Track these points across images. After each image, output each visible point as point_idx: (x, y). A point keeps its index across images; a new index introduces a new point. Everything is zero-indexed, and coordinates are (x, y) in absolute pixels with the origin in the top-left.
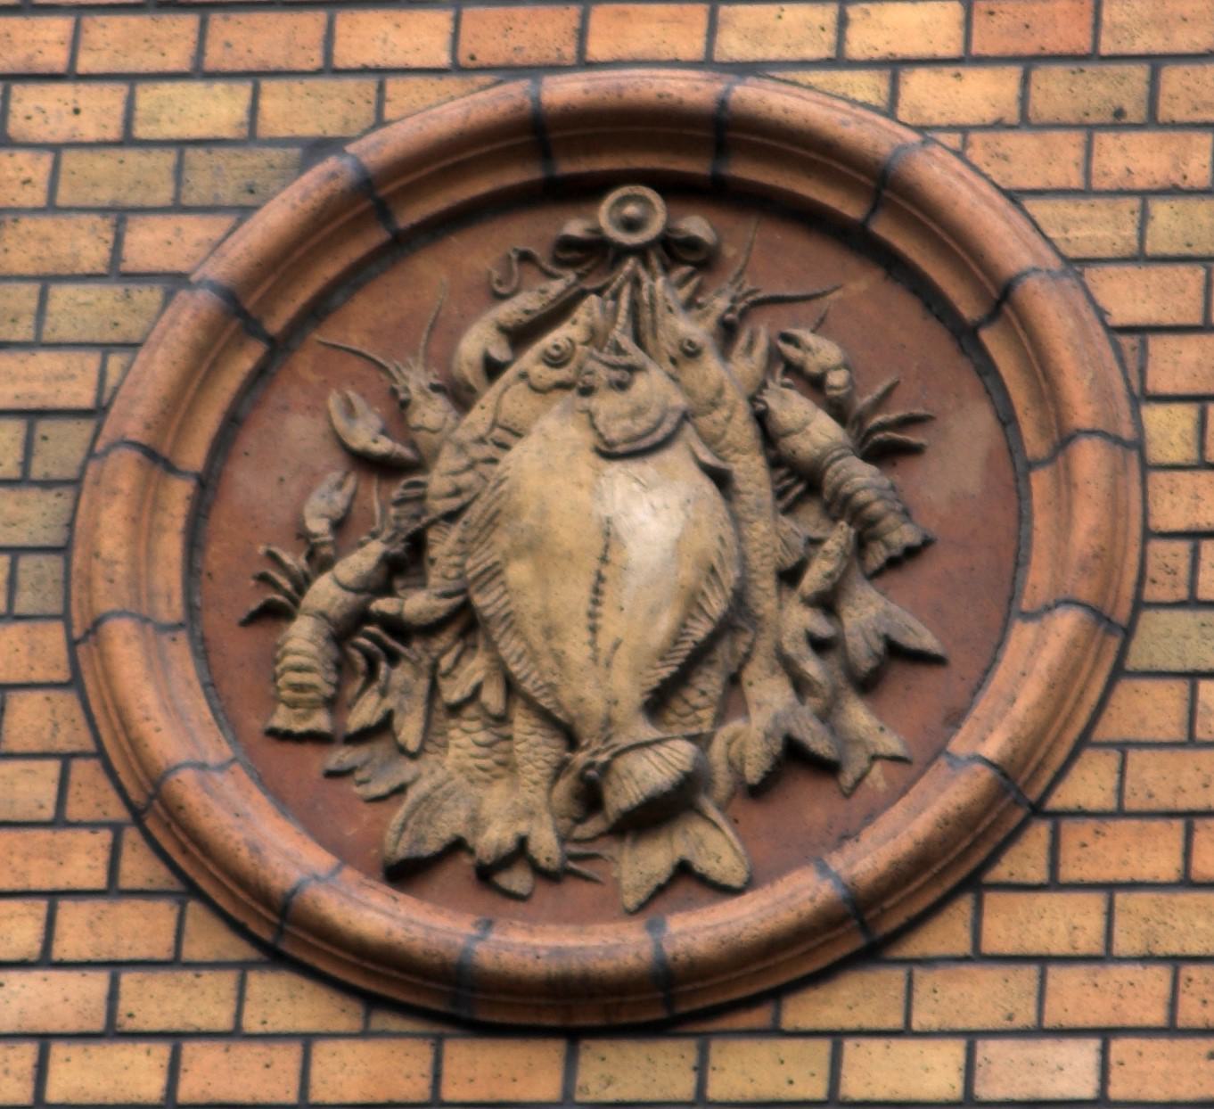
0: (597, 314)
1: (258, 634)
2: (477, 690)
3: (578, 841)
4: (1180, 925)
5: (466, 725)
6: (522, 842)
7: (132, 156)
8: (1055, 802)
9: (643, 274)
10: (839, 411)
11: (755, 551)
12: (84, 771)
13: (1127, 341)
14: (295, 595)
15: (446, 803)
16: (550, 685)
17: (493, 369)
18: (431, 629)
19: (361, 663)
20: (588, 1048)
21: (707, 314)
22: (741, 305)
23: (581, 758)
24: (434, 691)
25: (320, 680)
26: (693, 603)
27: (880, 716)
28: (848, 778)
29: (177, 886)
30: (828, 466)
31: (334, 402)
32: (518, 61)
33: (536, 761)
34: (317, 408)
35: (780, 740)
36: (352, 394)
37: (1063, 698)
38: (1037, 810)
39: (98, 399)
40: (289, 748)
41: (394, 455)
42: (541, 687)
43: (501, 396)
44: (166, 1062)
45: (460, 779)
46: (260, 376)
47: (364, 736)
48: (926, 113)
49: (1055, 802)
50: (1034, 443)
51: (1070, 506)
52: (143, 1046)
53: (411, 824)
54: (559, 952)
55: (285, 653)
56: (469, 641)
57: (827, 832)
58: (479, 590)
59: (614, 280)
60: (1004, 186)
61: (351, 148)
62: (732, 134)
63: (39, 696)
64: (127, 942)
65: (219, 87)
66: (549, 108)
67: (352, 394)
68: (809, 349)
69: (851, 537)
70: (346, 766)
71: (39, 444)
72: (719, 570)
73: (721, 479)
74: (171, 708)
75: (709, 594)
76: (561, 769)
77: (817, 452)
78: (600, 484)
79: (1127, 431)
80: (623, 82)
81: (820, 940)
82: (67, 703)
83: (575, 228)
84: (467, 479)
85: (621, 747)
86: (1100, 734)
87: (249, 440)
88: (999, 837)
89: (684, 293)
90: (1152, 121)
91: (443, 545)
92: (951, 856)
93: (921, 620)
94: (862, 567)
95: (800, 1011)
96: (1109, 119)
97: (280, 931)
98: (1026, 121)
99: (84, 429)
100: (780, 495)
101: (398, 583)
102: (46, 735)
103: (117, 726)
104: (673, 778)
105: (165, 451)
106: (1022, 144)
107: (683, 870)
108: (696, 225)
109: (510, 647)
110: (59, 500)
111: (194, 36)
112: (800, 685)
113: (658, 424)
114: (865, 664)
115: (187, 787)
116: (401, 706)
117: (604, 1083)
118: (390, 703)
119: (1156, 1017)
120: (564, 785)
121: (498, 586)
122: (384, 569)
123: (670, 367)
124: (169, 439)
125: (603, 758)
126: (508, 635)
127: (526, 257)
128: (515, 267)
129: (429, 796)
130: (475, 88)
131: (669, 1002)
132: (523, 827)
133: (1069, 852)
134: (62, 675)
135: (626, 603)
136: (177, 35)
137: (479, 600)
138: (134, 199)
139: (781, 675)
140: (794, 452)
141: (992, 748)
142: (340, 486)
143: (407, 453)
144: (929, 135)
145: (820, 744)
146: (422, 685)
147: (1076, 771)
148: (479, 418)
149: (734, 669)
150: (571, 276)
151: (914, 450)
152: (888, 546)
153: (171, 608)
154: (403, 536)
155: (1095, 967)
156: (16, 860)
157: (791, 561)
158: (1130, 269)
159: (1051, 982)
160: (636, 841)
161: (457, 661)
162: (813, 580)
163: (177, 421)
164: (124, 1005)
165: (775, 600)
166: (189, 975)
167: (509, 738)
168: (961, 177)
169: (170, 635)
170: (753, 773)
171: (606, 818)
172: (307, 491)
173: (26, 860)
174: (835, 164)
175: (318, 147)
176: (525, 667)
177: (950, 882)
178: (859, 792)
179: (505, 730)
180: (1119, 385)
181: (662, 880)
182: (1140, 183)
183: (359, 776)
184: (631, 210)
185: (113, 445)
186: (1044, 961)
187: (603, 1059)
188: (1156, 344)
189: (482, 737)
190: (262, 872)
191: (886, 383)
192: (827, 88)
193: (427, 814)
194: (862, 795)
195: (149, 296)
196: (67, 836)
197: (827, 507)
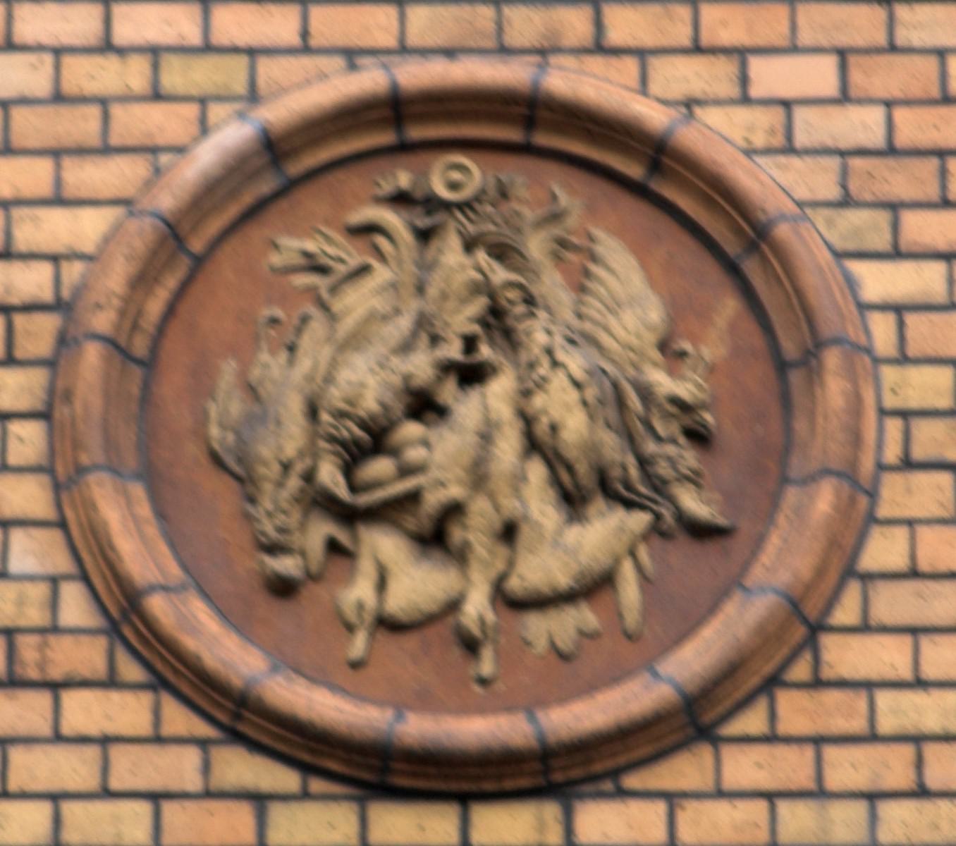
95: (632, 781)
97: (237, 717)
103: (95, 549)
115: (157, 605)
141: (783, 578)
153: (131, 460)
174: (632, 143)
184: (456, 176)
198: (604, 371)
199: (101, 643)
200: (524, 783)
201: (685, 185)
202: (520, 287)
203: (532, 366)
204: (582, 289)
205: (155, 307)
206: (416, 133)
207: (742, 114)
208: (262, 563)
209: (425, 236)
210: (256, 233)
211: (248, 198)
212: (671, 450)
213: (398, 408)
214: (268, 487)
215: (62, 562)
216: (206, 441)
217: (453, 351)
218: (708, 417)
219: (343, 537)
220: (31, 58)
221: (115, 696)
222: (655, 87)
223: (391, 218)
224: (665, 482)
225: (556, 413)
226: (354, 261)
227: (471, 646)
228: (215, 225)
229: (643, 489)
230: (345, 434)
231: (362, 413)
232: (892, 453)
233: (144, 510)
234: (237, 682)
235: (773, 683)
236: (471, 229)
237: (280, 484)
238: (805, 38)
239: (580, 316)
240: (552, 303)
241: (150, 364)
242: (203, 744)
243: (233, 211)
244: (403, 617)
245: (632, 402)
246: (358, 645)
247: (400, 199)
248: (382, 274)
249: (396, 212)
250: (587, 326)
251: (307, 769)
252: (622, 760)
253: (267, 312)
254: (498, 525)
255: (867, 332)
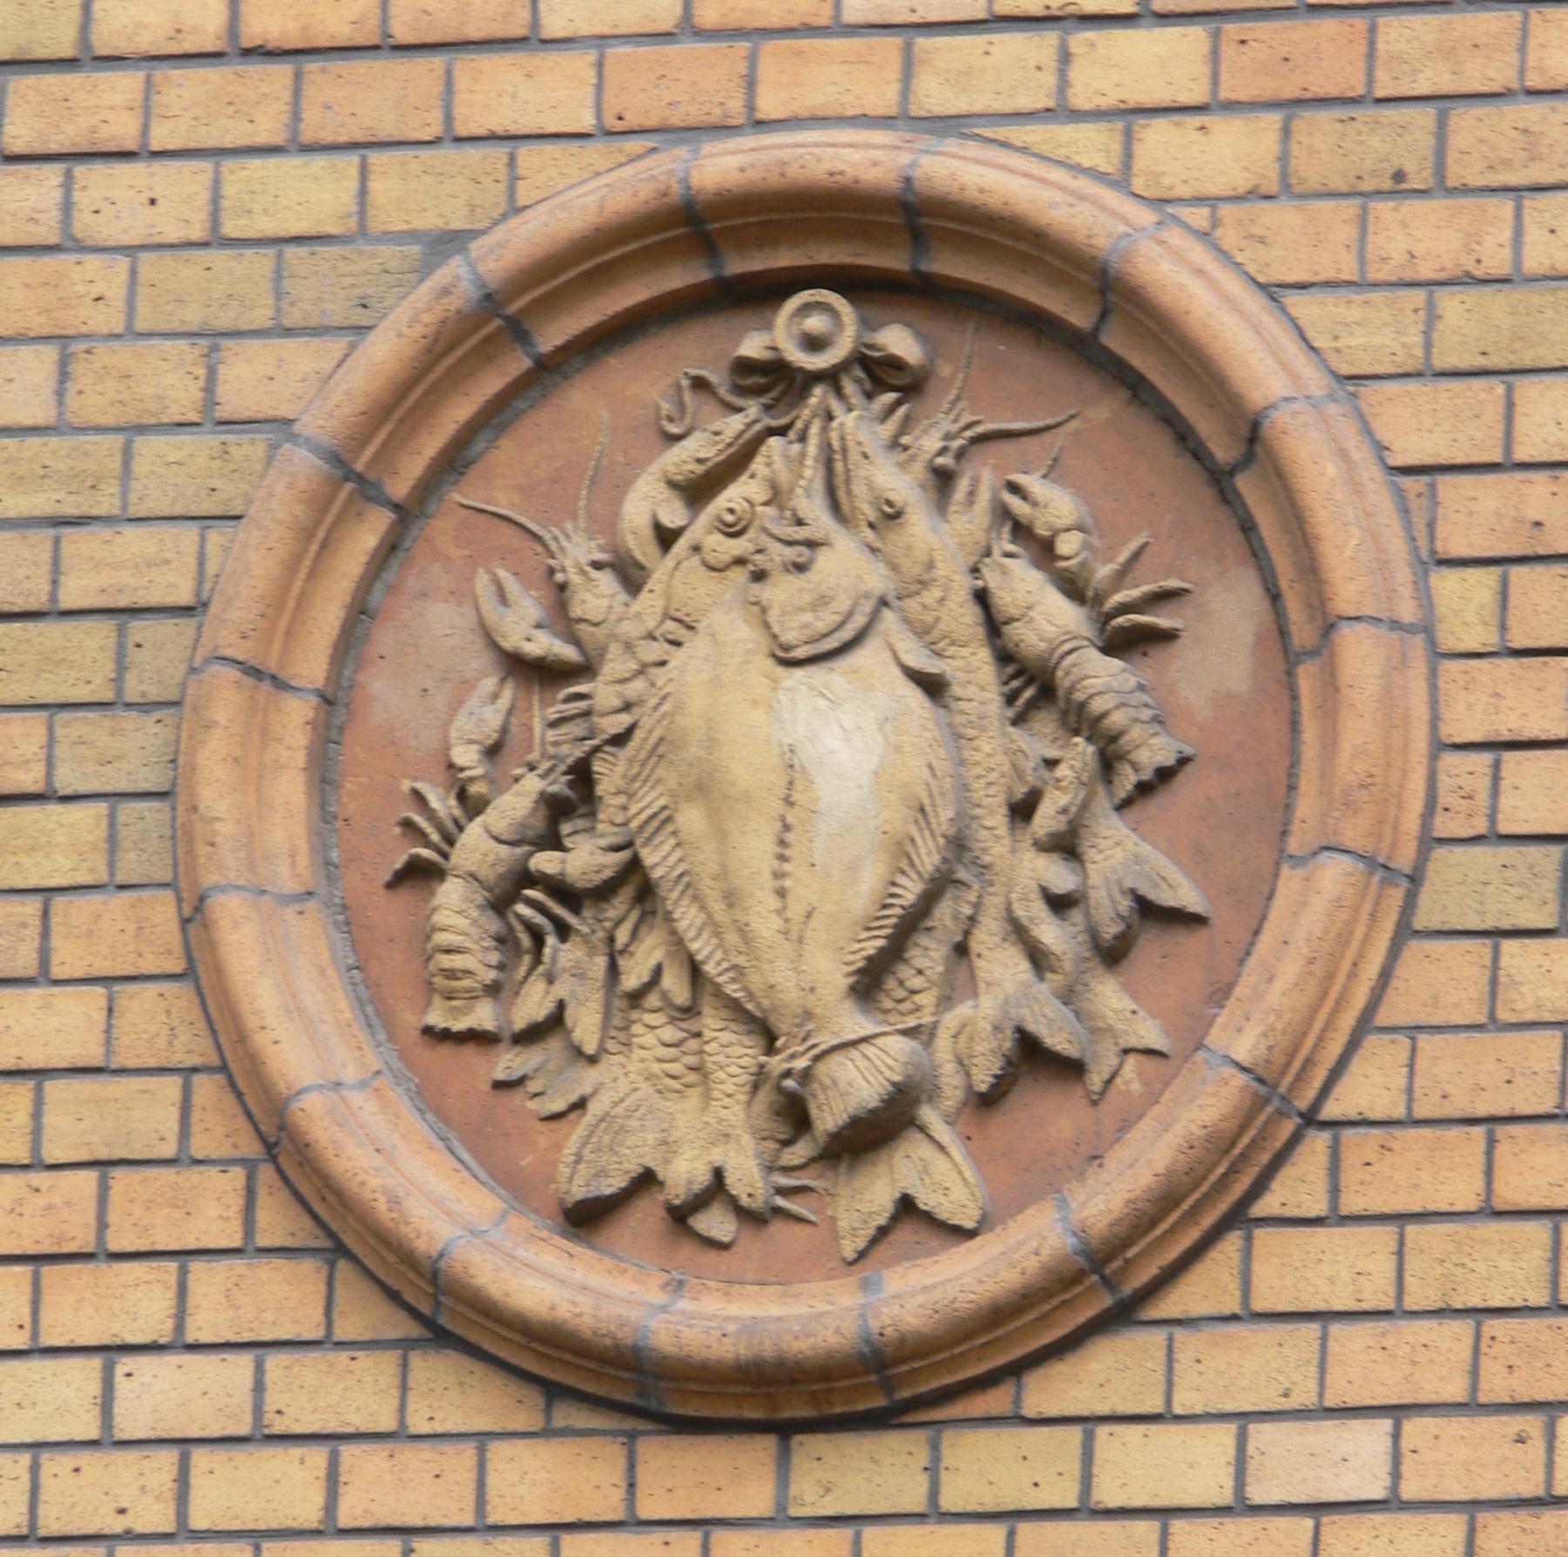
0: (779, 464)
1: (404, 899)
2: (658, 972)
3: (787, 1170)
4: (1481, 1267)
5: (649, 1018)
6: (718, 1174)
7: (220, 258)
8: (1330, 1111)
9: (836, 406)
10: (1073, 587)
11: (979, 777)
12: (206, 1089)
13: (1410, 483)
14: (444, 847)
15: (629, 1123)
16: (735, 967)
17: (666, 538)
18: (604, 892)
19: (525, 940)
20: (801, 1444)
21: (913, 458)
22: (957, 444)
23: (776, 1064)
24: (613, 971)
25: (479, 962)
26: (902, 852)
27: (1134, 995)
28: (1095, 1080)
29: (325, 1243)
30: (1058, 663)
31: (482, 581)
32: (675, 121)
33: (728, 1066)
34: (463, 593)
35: (1009, 1033)
36: (503, 574)
37: (1330, 976)
38: (1310, 1119)
39: (198, 593)
40: (445, 1050)
41: (551, 658)
42: (727, 970)
43: (671, 575)
44: (322, 1473)
45: (646, 1089)
46: (391, 548)
47: (531, 1035)
48: (1167, 180)
49: (1330, 1111)
50: (1302, 632)
51: (1335, 722)
52: (296, 1451)
53: (586, 1151)
54: (751, 1327)
55: (435, 929)
56: (648, 907)
57: (1073, 1150)
58: (645, 844)
59: (797, 417)
60: (1261, 279)
61: (476, 247)
62: (923, 220)
63: (152, 989)
64: (269, 1316)
65: (319, 162)
66: (699, 191)
67: (503, 574)
68: (1035, 504)
69: (1089, 759)
70: (515, 1075)
71: (133, 655)
72: (929, 809)
73: (932, 686)
74: (294, 1009)
75: (919, 840)
76: (759, 1078)
77: (1043, 645)
78: (778, 702)
79: (1407, 611)
80: (786, 154)
81: (1055, 1302)
82: (180, 996)
83: (753, 346)
84: (637, 687)
85: (823, 1047)
86: (1383, 1017)
87: (384, 639)
88: (1265, 1158)
89: (891, 426)
90: (1440, 187)
91: (610, 775)
92: (1204, 1188)
93: (1178, 863)
94: (1111, 794)
96: (1387, 184)
98: (1287, 189)
99: (183, 629)
100: (1010, 699)
101: (565, 828)
102: (162, 1042)
104: (882, 1092)
105: (271, 665)
106: (1280, 218)
107: (906, 1207)
108: (898, 341)
109: (687, 918)
110: (158, 729)
111: (286, 95)
112: (1038, 958)
113: (848, 616)
114: (1110, 930)
116: (573, 993)
117: (821, 1491)
118: (561, 990)
119: (1455, 1390)
120: (765, 1096)
121: (668, 837)
122: (543, 812)
123: (869, 534)
124: (276, 648)
125: (801, 1063)
126: (685, 902)
127: (700, 384)
128: (688, 397)
129: (607, 1114)
130: (623, 160)
131: (888, 1386)
132: (717, 1156)
133: (1352, 1174)
134: (176, 965)
135: (817, 858)
136: (266, 95)
137: (649, 857)
138: (224, 321)
139: (1013, 944)
140: (1017, 645)
141: (1245, 1048)
142: (495, 696)
143: (569, 653)
144: (1170, 210)
145: (1058, 1039)
146: (601, 962)
147: (1357, 1066)
148: (649, 603)
149: (959, 938)
150: (753, 408)
151: (1168, 636)
152: (1136, 767)
154: (563, 768)
155: (1383, 1325)
156: (138, 1210)
157: (1020, 791)
158: (1412, 386)
159: (1333, 1347)
160: (852, 1167)
161: (634, 935)
162: (1046, 818)
163: (283, 624)
164: (272, 1400)
165: (1007, 841)
166: (343, 1356)
167: (698, 1035)
168: (1200, 272)
169: (297, 907)
170: (983, 1082)
171: (814, 1140)
172: (457, 704)
173: (148, 1209)
175: (448, 242)
176: (706, 944)
177: (1208, 1220)
178: (1109, 1097)
179: (693, 1025)
180: (1397, 546)
181: (882, 1220)
182: (1426, 272)
183: (533, 1086)
184: (816, 323)
185: (207, 661)
186: (1324, 1317)
187: (819, 1459)
188: (1448, 486)
189: (670, 1033)
190: (403, 1229)
191: (1133, 546)
192: (1045, 149)
193: (607, 1139)
194: (1112, 1101)
195: (249, 448)
196: (194, 1175)
197: (1064, 715)
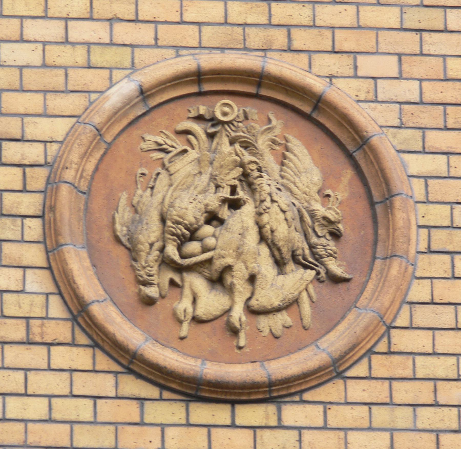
95: (307, 396)
184: (226, 109)
198: (294, 205)
199: (69, 324)
200: (260, 396)
201: (329, 117)
202: (256, 163)
203: (262, 201)
204: (282, 164)
205: (90, 167)
206: (207, 87)
207: (354, 83)
208: (140, 290)
209: (211, 136)
210: (135, 132)
211: (131, 117)
212: (323, 241)
213: (202, 220)
214: (143, 254)
215: (50, 287)
216: (114, 231)
217: (226, 193)
218: (340, 226)
219: (177, 279)
220: (32, 46)
221: (75, 350)
222: (315, 69)
223: (197, 127)
224: (321, 257)
225: (274, 225)
226: (180, 148)
227: (235, 332)
228: (117, 128)
229: (311, 260)
230: (179, 232)
231: (186, 222)
232: (423, 247)
233: (87, 263)
234: (132, 347)
235: (370, 352)
236: (233, 134)
237: (149, 253)
238: (383, 48)
239: (282, 177)
240: (269, 170)
241: (88, 193)
242: (116, 373)
243: (125, 122)
244: (204, 317)
245: (306, 218)
246: (185, 329)
247: (199, 118)
248: (193, 154)
249: (197, 123)
250: (285, 181)
251: (163, 387)
252: (303, 387)
253: (140, 171)
254: (247, 276)
255: (411, 188)
